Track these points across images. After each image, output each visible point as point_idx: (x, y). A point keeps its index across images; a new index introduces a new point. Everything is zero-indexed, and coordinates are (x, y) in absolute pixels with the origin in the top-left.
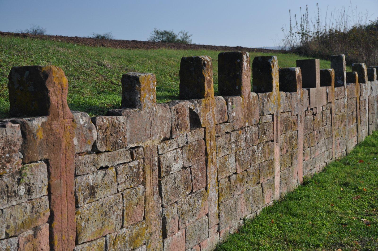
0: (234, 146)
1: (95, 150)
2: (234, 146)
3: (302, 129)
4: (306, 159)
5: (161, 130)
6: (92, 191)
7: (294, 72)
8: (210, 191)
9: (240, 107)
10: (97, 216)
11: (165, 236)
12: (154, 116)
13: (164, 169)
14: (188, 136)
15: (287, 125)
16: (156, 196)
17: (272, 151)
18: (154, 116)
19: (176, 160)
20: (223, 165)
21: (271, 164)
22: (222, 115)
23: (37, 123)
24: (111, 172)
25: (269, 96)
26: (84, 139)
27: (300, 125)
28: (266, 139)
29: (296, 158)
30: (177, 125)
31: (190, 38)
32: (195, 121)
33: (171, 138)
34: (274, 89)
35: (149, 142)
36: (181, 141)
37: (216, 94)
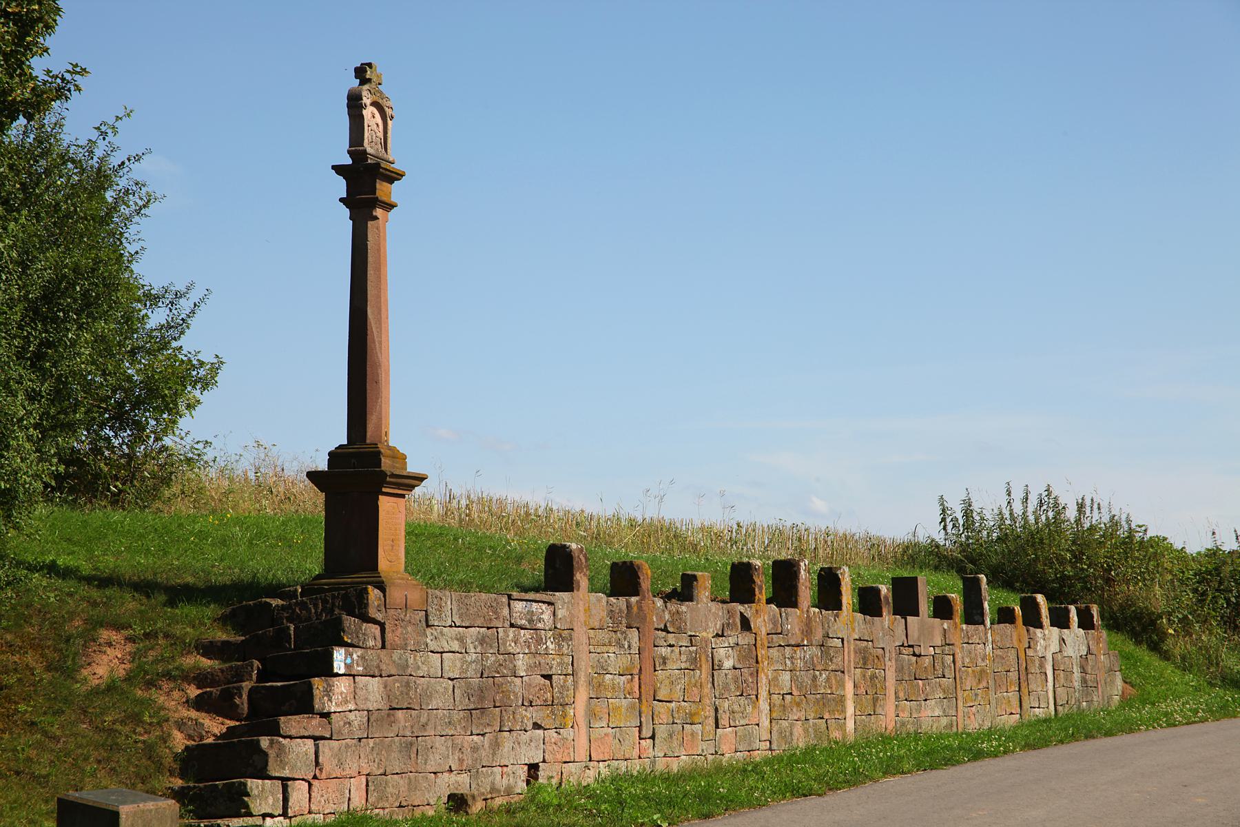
0: (788, 662)
1: (665, 630)
2: (788, 662)
3: (893, 669)
4: (901, 714)
5: (715, 626)
6: (664, 660)
7: (878, 591)
8: (761, 701)
9: (796, 621)
10: (667, 682)
11: (717, 727)
12: (706, 613)
13: (716, 662)
14: (736, 637)
15: (865, 659)
16: (710, 685)
17: (842, 685)
18: (706, 613)
19: (728, 657)
20: (776, 679)
21: (842, 700)
22: (775, 624)
23: (634, 599)
24: (677, 650)
25: (837, 615)
26: (660, 618)
27: (888, 663)
28: (833, 667)
29: (883, 707)
30: (728, 624)
31: (137, 171)
32: (746, 625)
33: (723, 636)
34: (844, 608)
35: (704, 634)
36: (732, 641)
37: (769, 601)
